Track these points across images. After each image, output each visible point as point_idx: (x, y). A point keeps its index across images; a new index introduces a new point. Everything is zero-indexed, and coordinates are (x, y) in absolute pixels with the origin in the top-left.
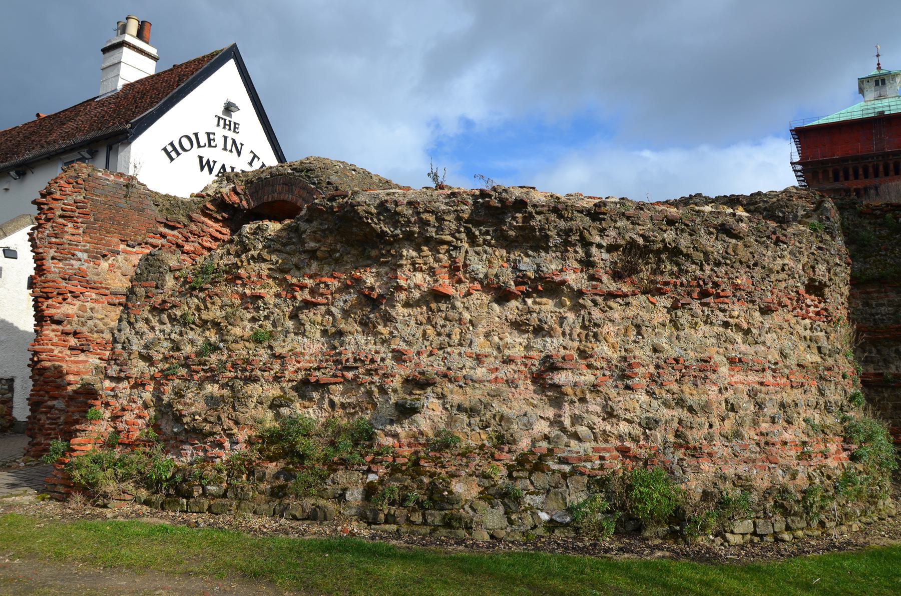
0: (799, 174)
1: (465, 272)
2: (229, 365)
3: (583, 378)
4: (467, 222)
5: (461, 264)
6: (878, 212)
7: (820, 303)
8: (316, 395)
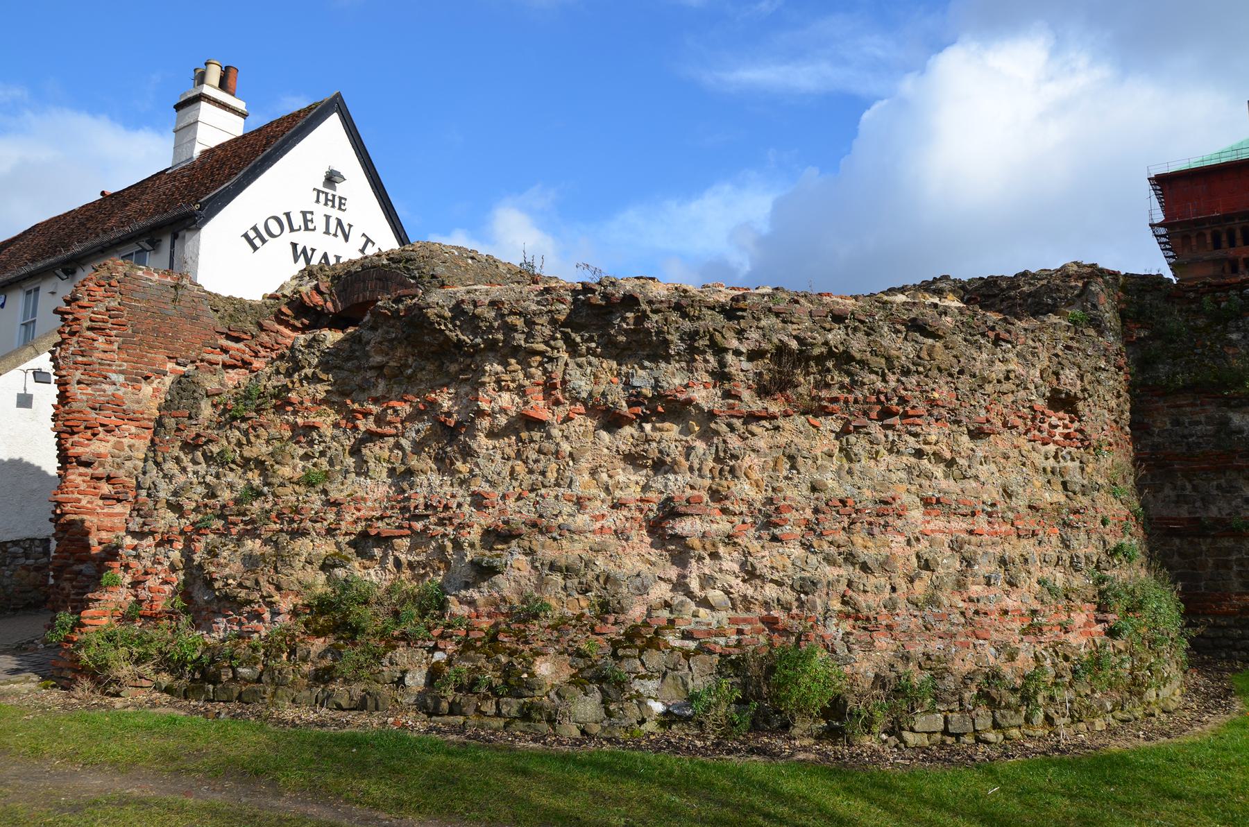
0: (1164, 240)
1: (564, 391)
2: (274, 514)
3: (715, 526)
4: (564, 324)
5: (558, 381)
6: (1192, 295)
7: (1072, 421)
8: (377, 552)
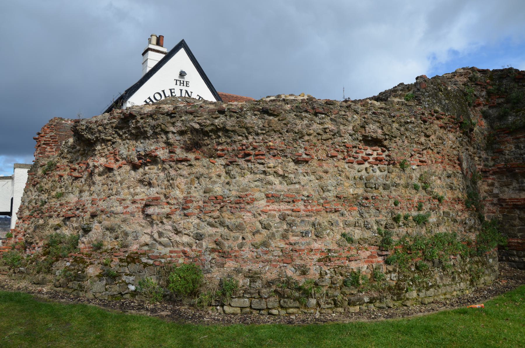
3: (163, 210)
4: (116, 128)
